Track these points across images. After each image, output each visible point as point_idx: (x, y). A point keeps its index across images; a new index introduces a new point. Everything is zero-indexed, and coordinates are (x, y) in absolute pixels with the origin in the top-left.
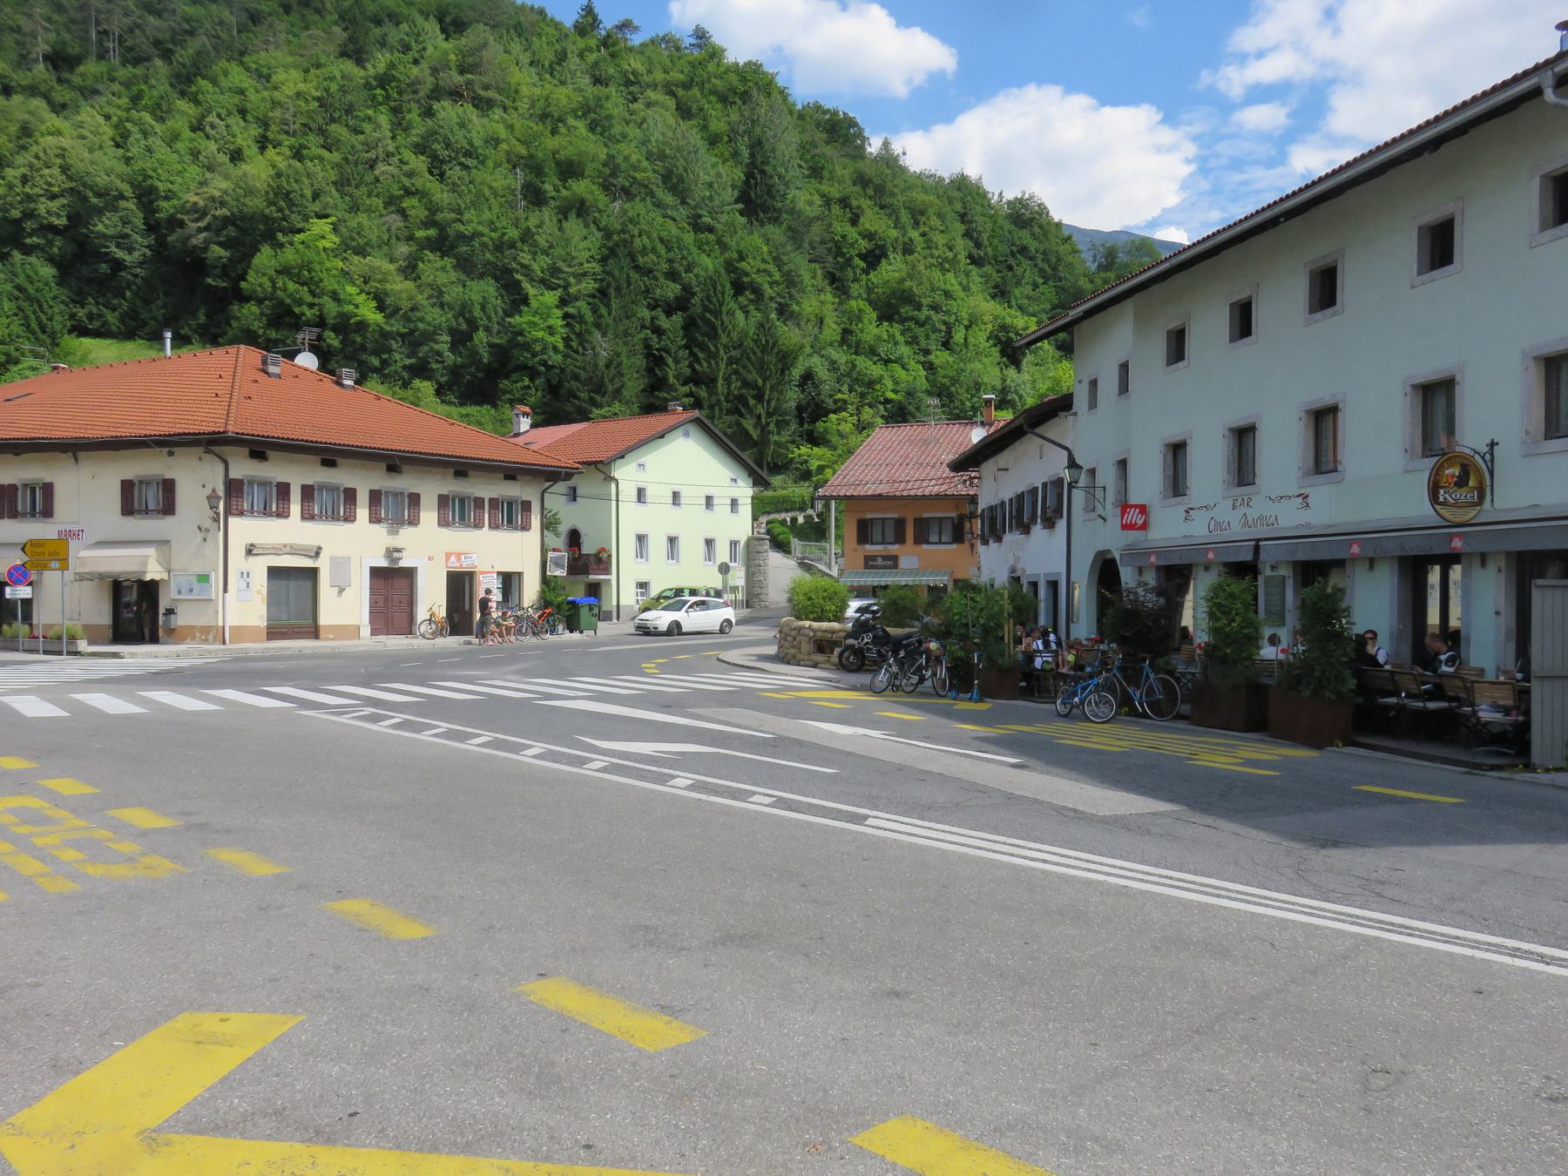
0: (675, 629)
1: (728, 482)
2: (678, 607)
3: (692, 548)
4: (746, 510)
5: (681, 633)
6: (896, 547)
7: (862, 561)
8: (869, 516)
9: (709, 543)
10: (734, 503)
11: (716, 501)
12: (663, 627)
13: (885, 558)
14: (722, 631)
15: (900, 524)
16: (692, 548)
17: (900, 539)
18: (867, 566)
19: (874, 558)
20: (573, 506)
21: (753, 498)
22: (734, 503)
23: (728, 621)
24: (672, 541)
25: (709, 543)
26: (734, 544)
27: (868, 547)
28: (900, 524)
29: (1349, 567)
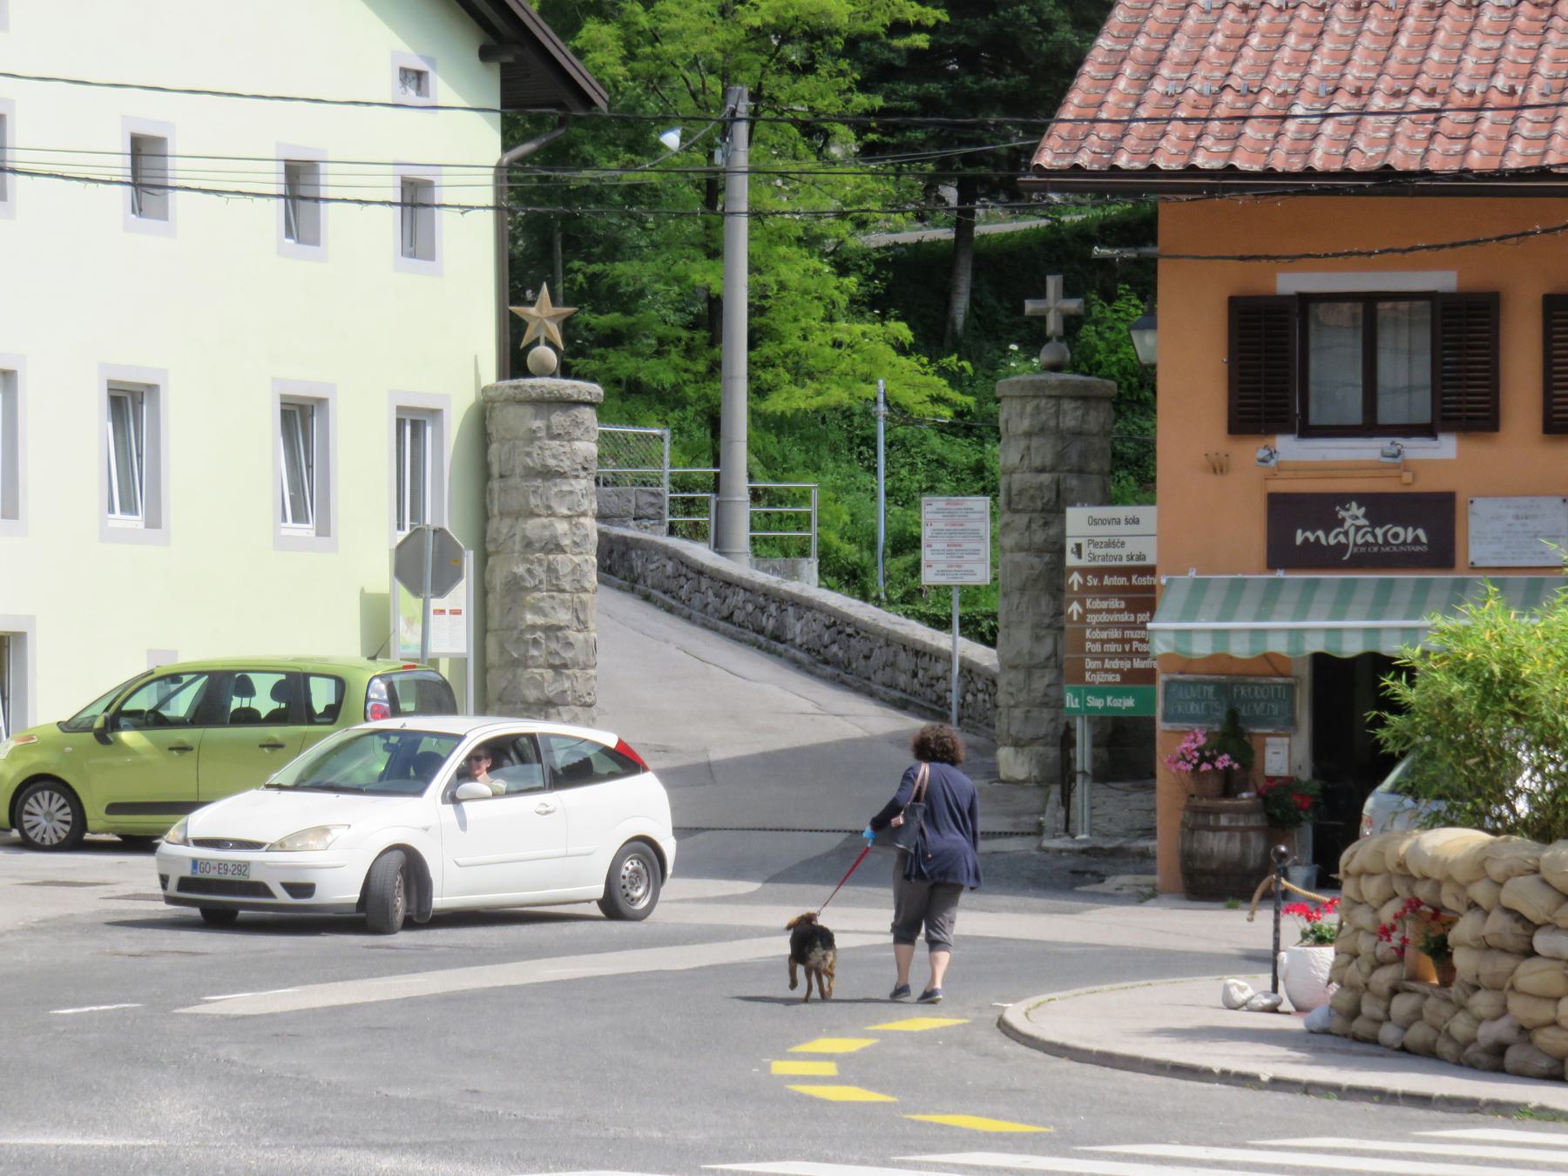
0: (400, 900)
1: (386, 86)
2: (409, 767)
3: (218, 448)
4: (471, 244)
5: (424, 918)
6: (1446, 447)
7: (1253, 532)
8: (1290, 282)
9: (300, 419)
10: (415, 198)
11: (331, 182)
12: (341, 885)
13: (1382, 507)
14: (613, 907)
15: (1465, 325)
16: (218, 448)
17: (1466, 405)
18: (1281, 554)
19: (1323, 508)
20: (146, 237)
21: (507, 176)
22: (415, 198)
23: (644, 848)
24: (127, 404)
25: (300, 419)
26: (413, 424)
27: (1288, 447)
28: (1465, 325)
29: (1397, 1045)
